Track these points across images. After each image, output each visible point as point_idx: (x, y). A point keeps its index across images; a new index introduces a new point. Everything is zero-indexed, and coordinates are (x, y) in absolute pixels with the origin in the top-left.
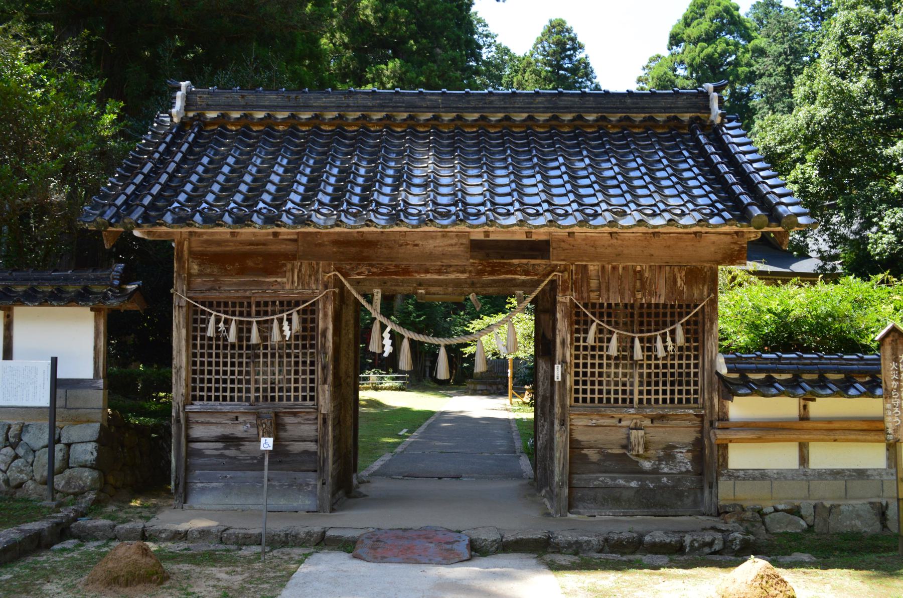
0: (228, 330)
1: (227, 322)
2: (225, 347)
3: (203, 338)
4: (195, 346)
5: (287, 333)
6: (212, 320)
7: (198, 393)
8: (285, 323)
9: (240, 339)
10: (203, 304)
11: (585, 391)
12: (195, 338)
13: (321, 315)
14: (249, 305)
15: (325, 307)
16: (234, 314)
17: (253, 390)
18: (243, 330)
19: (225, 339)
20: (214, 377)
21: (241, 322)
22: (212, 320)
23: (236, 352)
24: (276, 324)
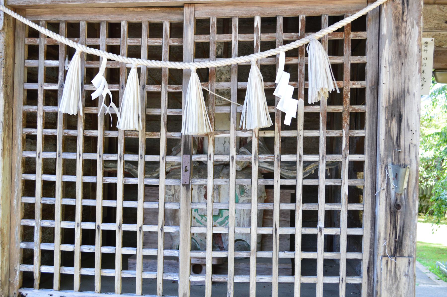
0: (115, 98)
1: (113, 76)
2: (111, 146)
3: (51, 122)
4: (30, 140)
5: (290, 107)
6: (74, 68)
7: (36, 268)
8: (282, 77)
9: (152, 122)
10: (54, 27)
11: (332, 219)
12: (30, 121)
13: (387, 54)
14: (177, 30)
15: (398, 31)
16: (134, 53)
17: (185, 266)
18: (164, 92)
19: (111, 122)
20: (78, 225)
21: (154, 76)
22: (74, 68)
23: (141, 158)
24: (255, 83)
